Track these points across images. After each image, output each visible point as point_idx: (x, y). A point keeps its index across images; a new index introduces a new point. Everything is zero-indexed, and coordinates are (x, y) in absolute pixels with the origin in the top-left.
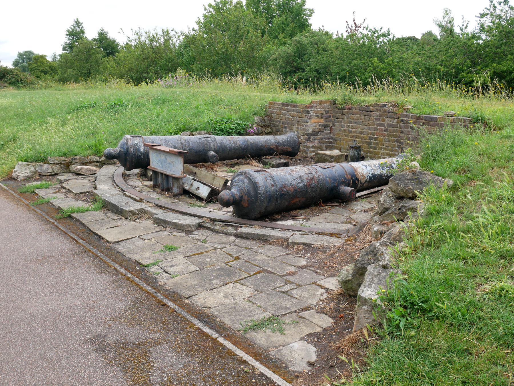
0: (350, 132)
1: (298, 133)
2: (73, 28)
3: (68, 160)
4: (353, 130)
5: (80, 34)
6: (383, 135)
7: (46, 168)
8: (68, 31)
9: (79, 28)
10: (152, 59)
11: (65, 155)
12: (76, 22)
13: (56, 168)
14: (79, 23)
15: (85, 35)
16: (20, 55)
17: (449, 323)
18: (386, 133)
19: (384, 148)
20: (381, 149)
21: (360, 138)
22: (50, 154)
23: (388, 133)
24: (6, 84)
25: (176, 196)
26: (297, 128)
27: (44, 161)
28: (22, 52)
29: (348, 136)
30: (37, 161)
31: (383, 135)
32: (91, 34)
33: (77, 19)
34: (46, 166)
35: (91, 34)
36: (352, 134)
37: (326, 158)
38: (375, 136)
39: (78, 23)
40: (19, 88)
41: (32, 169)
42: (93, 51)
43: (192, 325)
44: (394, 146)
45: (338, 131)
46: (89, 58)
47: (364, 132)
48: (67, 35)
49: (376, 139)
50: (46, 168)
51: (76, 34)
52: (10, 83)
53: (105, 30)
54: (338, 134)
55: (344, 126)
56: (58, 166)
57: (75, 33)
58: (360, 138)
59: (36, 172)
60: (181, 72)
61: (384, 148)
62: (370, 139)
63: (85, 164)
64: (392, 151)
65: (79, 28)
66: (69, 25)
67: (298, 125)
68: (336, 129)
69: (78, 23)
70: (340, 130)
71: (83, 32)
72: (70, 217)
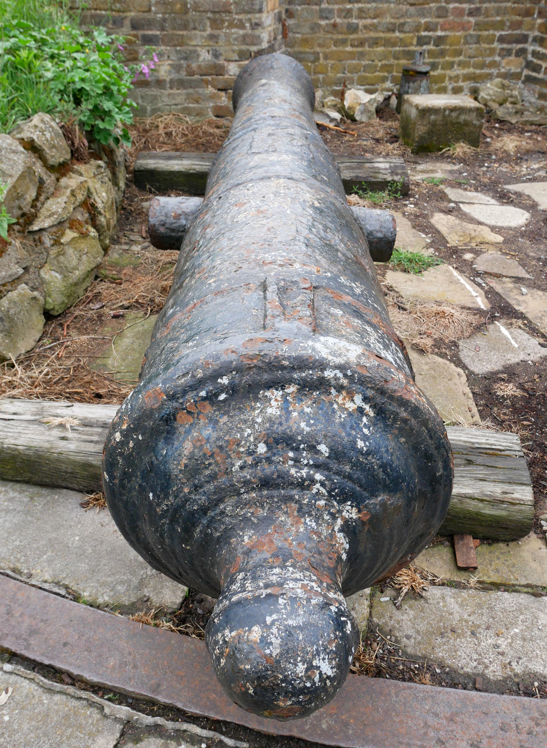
0: (353, 29)
1: (216, 55)
4: (361, 23)
6: (464, 27)
17: (57, 363)
18: (472, 20)
19: (460, 64)
20: (451, 65)
21: (388, 43)
23: (481, 18)
26: (212, 37)
29: (344, 42)
31: (464, 27)
36: (360, 35)
37: (463, 118)
38: (439, 33)
44: (492, 52)
45: (306, 30)
47: (403, 24)
49: (439, 41)
54: (305, 41)
55: (331, 11)
58: (388, 43)
61: (460, 64)
62: (421, 41)
64: (482, 66)
67: (216, 24)
68: (298, 26)
70: (315, 27)
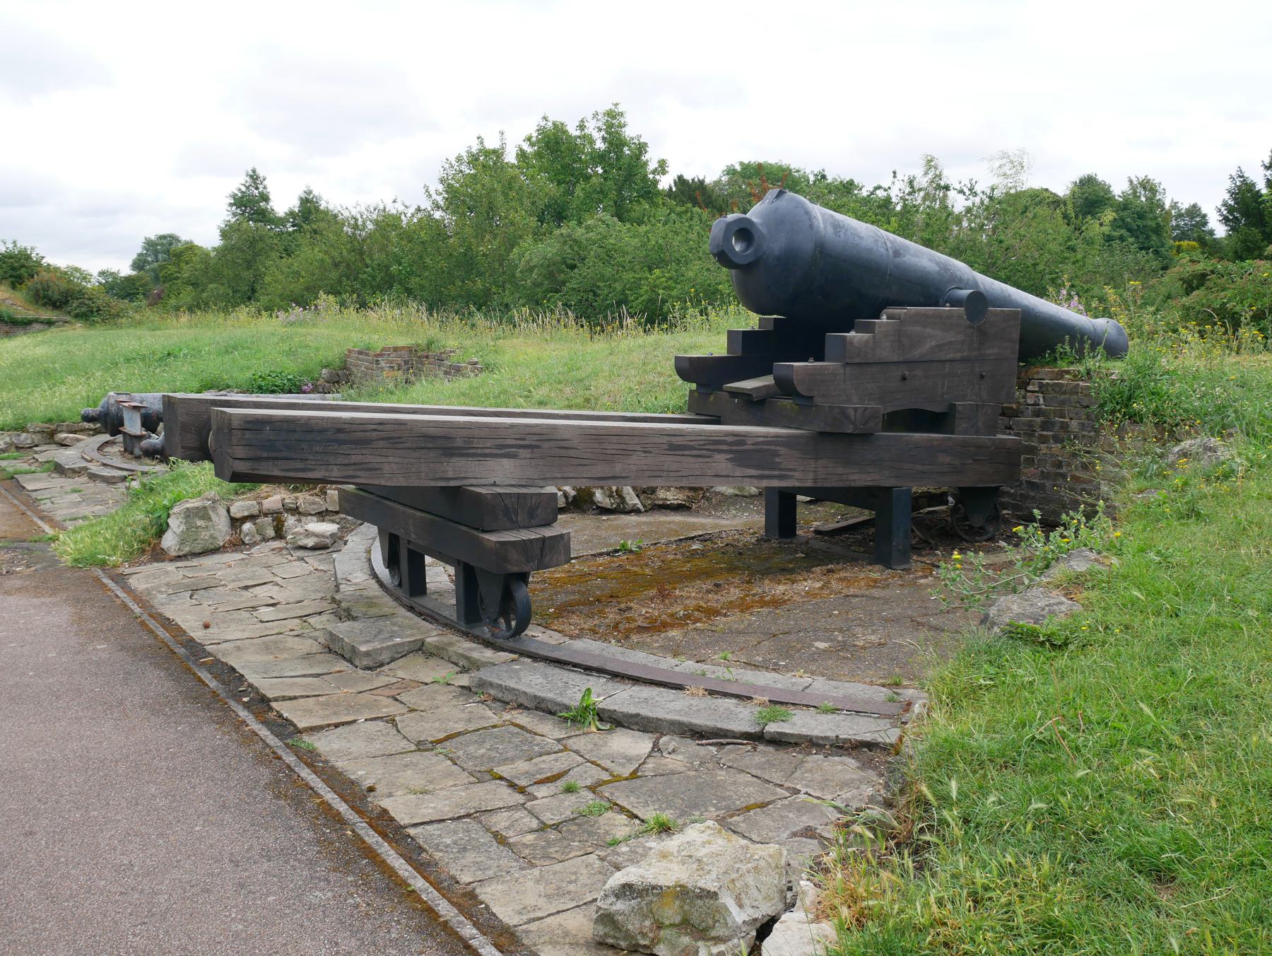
2: (244, 189)
3: (53, 427)
5: (258, 202)
7: (24, 438)
8: (234, 196)
9: (257, 188)
10: (348, 266)
11: (50, 421)
12: (251, 177)
13: (37, 438)
14: (258, 178)
15: (271, 204)
16: (150, 245)
22: (32, 420)
24: (68, 318)
25: (138, 458)
27: (23, 429)
28: (153, 238)
30: (16, 429)
32: (283, 202)
33: (254, 171)
34: (24, 435)
35: (283, 202)
39: (254, 177)
40: (93, 324)
41: (7, 439)
42: (260, 245)
43: (36, 524)
46: (272, 255)
48: (231, 205)
50: (24, 438)
51: (251, 204)
52: (77, 316)
53: (315, 192)
56: (39, 436)
57: (249, 201)
59: (11, 444)
60: (325, 300)
63: (75, 432)
65: (257, 188)
66: (236, 183)
69: (254, 177)
71: (265, 198)
72: (13, 478)
